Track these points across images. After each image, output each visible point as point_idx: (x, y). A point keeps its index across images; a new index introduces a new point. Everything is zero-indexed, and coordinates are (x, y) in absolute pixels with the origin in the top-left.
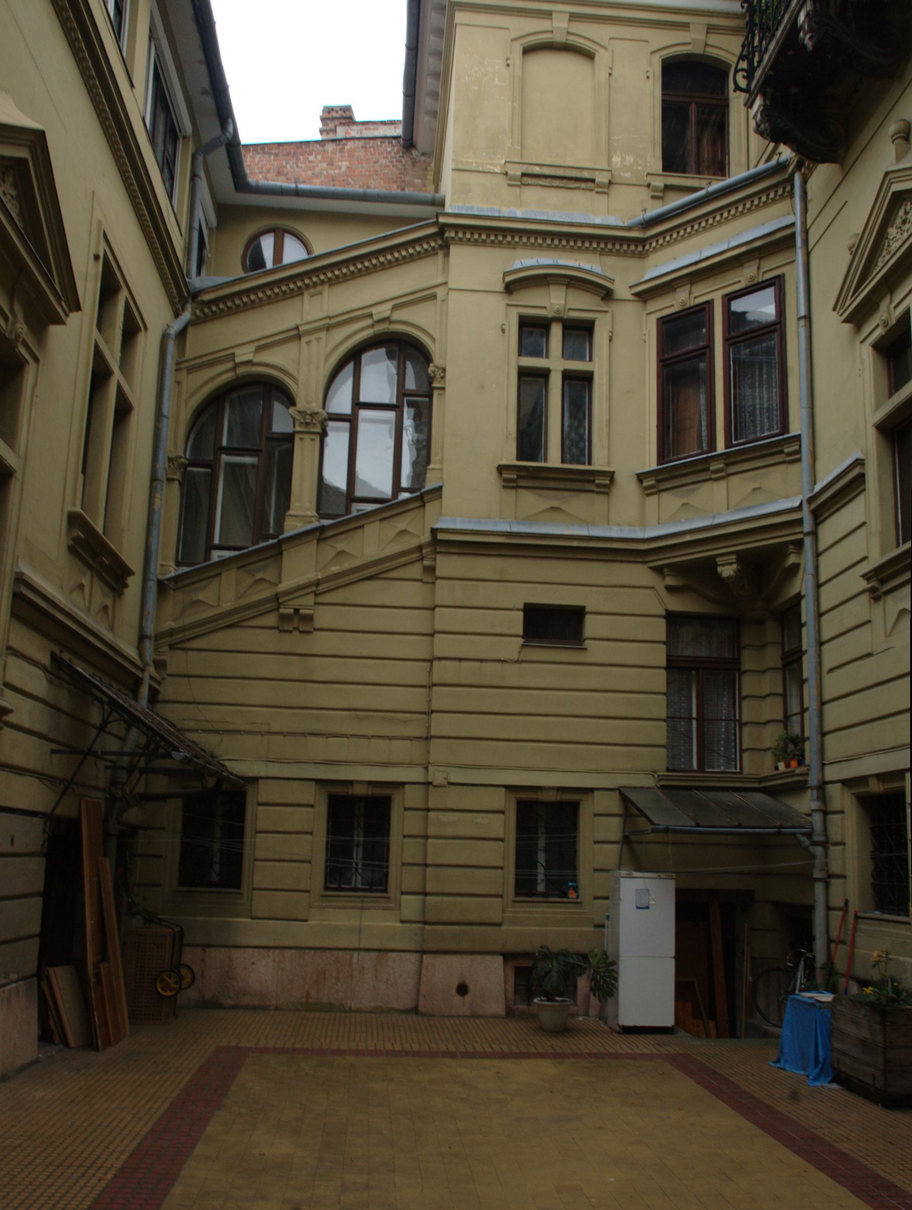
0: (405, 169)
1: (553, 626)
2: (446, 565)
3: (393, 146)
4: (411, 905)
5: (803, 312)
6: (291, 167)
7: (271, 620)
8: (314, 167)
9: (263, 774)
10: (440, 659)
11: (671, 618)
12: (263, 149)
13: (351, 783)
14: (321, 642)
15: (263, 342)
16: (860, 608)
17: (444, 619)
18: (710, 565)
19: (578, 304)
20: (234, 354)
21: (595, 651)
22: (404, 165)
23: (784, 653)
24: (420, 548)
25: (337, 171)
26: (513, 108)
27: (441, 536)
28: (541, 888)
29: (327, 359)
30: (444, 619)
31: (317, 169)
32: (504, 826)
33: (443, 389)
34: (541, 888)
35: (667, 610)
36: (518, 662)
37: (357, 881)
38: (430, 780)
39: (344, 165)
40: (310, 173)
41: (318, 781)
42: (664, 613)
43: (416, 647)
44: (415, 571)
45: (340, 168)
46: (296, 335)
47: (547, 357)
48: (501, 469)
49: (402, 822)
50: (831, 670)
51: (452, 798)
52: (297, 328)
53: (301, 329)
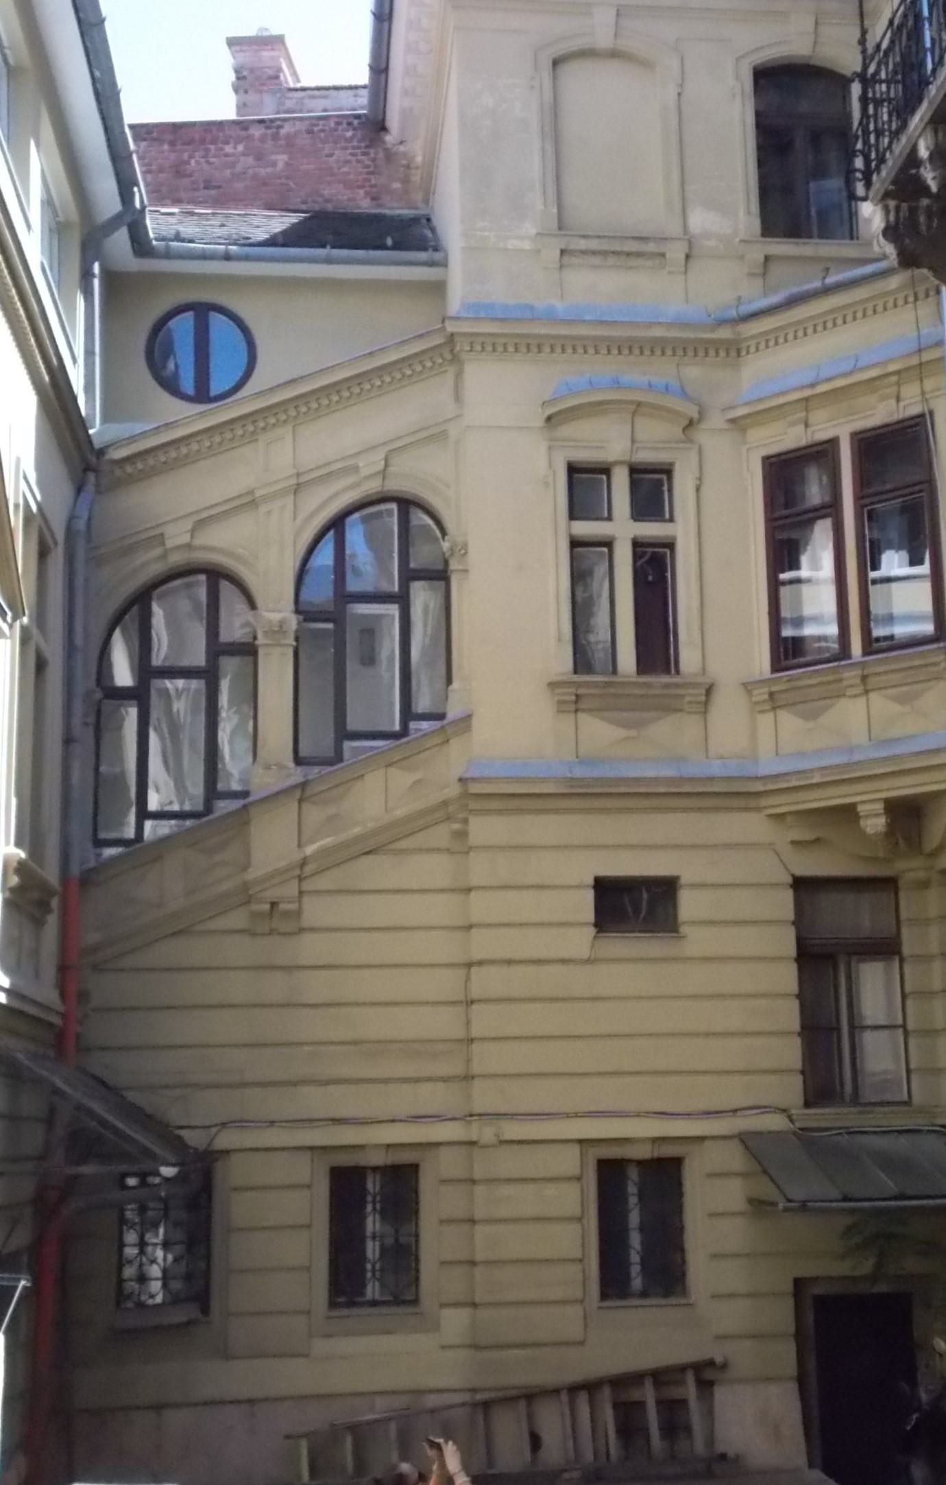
0: (376, 166)
1: (633, 905)
2: (484, 829)
3: (354, 129)
4: (455, 1322)
6: (198, 163)
7: (238, 919)
8: (233, 165)
9: (237, 1145)
10: (480, 963)
11: (801, 885)
12: (149, 133)
13: (361, 1147)
14: (310, 948)
15: (204, 515)
17: (481, 906)
18: (848, 813)
19: (653, 441)
20: (162, 534)
21: (695, 940)
22: (374, 160)
24: (445, 803)
25: (269, 170)
26: (543, 150)
27: (475, 788)
28: (637, 1283)
29: (297, 535)
31: (239, 168)
33: (466, 571)
35: (793, 875)
36: (589, 961)
37: (372, 1290)
38: (474, 1138)
39: (281, 159)
40: (228, 172)
42: (790, 880)
43: (444, 948)
44: (440, 835)
45: (274, 164)
46: (249, 502)
48: (553, 685)
49: (435, 1201)
51: (510, 1163)
52: (251, 492)
53: (258, 493)
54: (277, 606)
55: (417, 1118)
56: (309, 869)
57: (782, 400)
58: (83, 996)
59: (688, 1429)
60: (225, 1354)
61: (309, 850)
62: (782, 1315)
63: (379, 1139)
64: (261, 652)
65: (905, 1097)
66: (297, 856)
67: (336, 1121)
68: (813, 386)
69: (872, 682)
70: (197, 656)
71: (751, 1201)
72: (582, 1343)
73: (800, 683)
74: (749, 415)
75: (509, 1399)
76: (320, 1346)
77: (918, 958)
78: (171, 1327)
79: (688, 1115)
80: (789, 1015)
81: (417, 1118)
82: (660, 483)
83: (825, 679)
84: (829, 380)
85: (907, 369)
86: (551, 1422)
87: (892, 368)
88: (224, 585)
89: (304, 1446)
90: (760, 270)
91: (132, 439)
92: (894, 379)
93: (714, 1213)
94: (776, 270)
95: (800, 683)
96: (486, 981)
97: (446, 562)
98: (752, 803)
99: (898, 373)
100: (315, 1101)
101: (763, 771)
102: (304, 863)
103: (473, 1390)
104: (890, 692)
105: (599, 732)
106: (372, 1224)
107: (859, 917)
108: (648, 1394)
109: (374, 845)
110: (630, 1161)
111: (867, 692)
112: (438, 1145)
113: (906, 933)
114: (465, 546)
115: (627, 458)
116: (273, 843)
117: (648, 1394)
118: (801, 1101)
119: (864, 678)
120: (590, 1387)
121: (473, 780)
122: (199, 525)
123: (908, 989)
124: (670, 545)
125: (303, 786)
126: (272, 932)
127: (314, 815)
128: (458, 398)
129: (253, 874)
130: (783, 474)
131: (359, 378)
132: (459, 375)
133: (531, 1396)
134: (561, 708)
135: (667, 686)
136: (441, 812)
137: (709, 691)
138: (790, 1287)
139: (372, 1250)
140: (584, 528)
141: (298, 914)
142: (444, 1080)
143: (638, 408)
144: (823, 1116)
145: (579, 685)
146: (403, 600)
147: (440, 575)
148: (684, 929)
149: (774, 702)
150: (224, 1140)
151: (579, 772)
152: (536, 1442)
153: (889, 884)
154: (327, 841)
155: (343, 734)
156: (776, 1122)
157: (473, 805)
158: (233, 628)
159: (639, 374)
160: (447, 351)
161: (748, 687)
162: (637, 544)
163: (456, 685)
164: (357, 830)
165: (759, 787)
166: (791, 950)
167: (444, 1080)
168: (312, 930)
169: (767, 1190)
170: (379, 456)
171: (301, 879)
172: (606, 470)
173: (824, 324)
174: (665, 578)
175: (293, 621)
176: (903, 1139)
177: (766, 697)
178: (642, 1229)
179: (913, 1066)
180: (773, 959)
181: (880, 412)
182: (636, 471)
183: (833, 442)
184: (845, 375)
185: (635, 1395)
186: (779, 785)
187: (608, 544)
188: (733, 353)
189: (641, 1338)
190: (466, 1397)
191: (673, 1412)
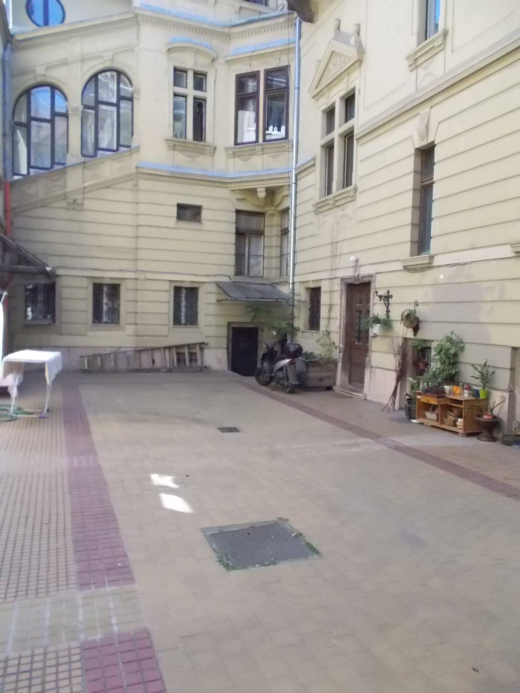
1: (188, 213)
2: (143, 184)
4: (130, 329)
5: (296, 86)
7: (63, 204)
13: (103, 278)
14: (88, 216)
16: (312, 217)
17: (142, 208)
18: (253, 191)
19: (202, 64)
23: (282, 229)
24: (131, 175)
27: (141, 170)
28: (183, 321)
30: (142, 208)
32: (169, 297)
34: (183, 321)
37: (105, 319)
41: (88, 277)
44: (129, 185)
46: (65, 63)
47: (186, 87)
48: (167, 140)
49: (125, 295)
50: (362, 161)
54: (75, 101)
55: (121, 271)
56: (86, 190)
57: (242, 56)
58: (12, 223)
59: (196, 360)
60: (60, 333)
61: (86, 184)
62: (224, 332)
63: (108, 276)
64: (70, 117)
65: (262, 275)
66: (83, 186)
67: (95, 269)
68: (254, 51)
69: (265, 151)
70: (48, 116)
71: (218, 301)
72: (168, 336)
73: (243, 149)
74: (232, 60)
75: (146, 350)
76: (90, 333)
77: (269, 236)
78: (43, 325)
79: (201, 276)
80: (232, 249)
81: (121, 271)
82: (202, 79)
83: (250, 149)
84: (259, 50)
85: (283, 50)
86: (158, 356)
87: (280, 49)
88: (57, 92)
89: (86, 360)
90: (238, 11)
91: (24, 33)
92: (279, 53)
93: (207, 304)
94: (244, 12)
95: (243, 149)
96: (143, 231)
97: (132, 95)
98: (226, 186)
99: (281, 51)
100: (88, 263)
101: (229, 176)
102: (84, 188)
103: (136, 348)
104: (271, 154)
105: (180, 159)
106: (105, 300)
107: (254, 223)
108: (186, 351)
109: (108, 185)
110: (183, 288)
111: (263, 154)
112: (126, 279)
113: (266, 229)
114: (139, 90)
115: (193, 68)
116: (74, 180)
117: (186, 351)
118: (233, 274)
119: (263, 149)
120: (170, 348)
121: (140, 167)
122: (48, 68)
123: (266, 245)
124: (205, 100)
125: (84, 163)
126: (74, 209)
127: (88, 173)
128: (138, 38)
129: (67, 190)
130: (241, 81)
131: (104, 25)
132: (138, 29)
133: (153, 349)
134: (169, 148)
135: (202, 145)
136: (129, 177)
137: (215, 149)
138: (226, 324)
139: (105, 308)
140: (179, 90)
141: (82, 204)
142: (129, 260)
143: (197, 51)
144: (239, 279)
145: (175, 141)
146: (117, 105)
147: (131, 99)
148: (203, 221)
149: (234, 155)
150: (59, 272)
151: (173, 170)
152: (153, 362)
153: (261, 214)
154: (92, 182)
155: (97, 148)
156: (226, 279)
157: (140, 176)
158: (60, 106)
159: (199, 40)
160: (135, 20)
161: (227, 149)
162: (195, 98)
163: (135, 136)
164: (102, 180)
165: (228, 181)
166: (234, 231)
167: (129, 260)
168: (88, 210)
169: (223, 297)
170: (111, 54)
171: (84, 193)
172: (185, 71)
173: (258, 31)
174: (202, 112)
175: (81, 108)
176: (261, 286)
177: (232, 153)
178: (186, 307)
179: (265, 267)
180: (228, 233)
181: (273, 64)
182: (196, 73)
183: (258, 72)
184: (263, 49)
185: (182, 351)
186: (234, 181)
187: (185, 96)
188: (228, 38)
189: (185, 336)
190: (133, 349)
191: (192, 356)
